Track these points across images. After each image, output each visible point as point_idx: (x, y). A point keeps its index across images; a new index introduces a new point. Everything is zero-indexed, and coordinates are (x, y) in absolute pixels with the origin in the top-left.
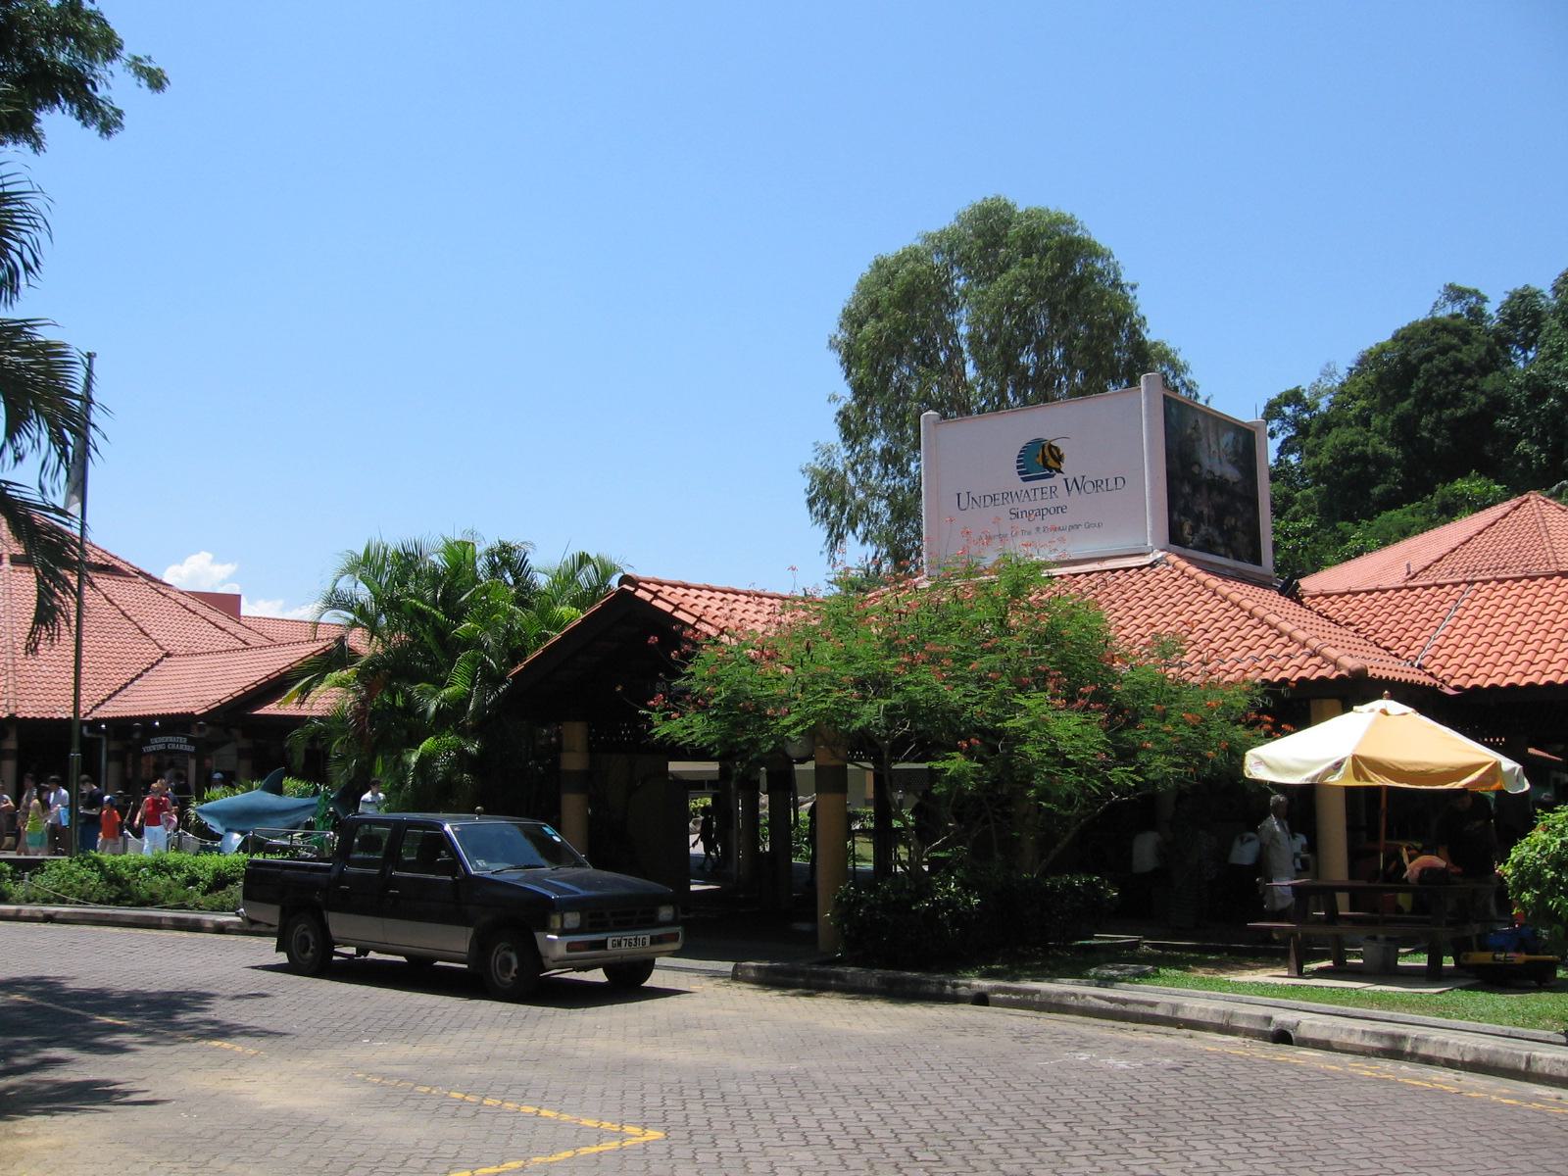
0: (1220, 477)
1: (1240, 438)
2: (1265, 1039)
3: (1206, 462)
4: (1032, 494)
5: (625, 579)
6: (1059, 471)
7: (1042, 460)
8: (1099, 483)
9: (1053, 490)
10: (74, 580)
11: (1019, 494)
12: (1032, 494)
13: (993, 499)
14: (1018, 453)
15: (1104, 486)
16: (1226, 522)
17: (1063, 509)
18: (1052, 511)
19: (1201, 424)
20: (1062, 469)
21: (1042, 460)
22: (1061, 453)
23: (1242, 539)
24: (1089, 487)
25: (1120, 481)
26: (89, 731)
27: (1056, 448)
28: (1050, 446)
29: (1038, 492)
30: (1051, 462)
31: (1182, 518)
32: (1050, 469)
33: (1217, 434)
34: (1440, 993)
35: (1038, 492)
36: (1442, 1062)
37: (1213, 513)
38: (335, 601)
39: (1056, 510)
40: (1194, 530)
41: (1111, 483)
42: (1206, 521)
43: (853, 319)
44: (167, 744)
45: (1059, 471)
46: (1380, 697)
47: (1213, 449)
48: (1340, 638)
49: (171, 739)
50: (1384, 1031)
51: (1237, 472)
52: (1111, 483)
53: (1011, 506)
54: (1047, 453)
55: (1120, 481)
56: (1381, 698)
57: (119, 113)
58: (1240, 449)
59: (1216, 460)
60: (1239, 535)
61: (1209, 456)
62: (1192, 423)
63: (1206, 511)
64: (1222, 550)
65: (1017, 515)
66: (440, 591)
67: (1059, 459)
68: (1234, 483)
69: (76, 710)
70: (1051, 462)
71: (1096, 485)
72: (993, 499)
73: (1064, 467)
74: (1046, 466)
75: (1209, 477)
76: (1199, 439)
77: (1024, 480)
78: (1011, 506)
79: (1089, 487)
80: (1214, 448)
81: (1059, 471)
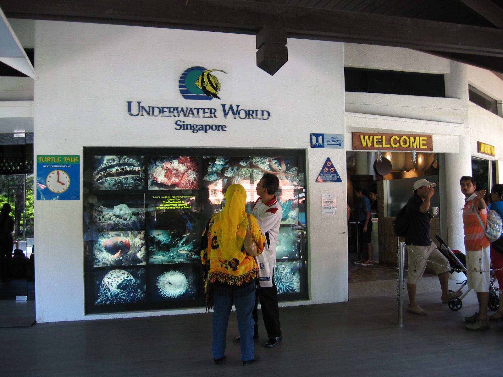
5: (153, 187)
10: (196, 250)
13: (161, 110)
15: (254, 115)
17: (222, 128)
20: (218, 95)
22: (434, 158)
24: (242, 114)
25: (266, 114)
27: (213, 77)
34: (276, 345)
36: (302, 176)
38: (32, 214)
41: (259, 114)
53: (177, 119)
54: (206, 79)
55: (266, 114)
66: (203, 207)
69: (502, 290)
71: (248, 113)
78: (177, 119)
79: (242, 114)
81: (216, 96)
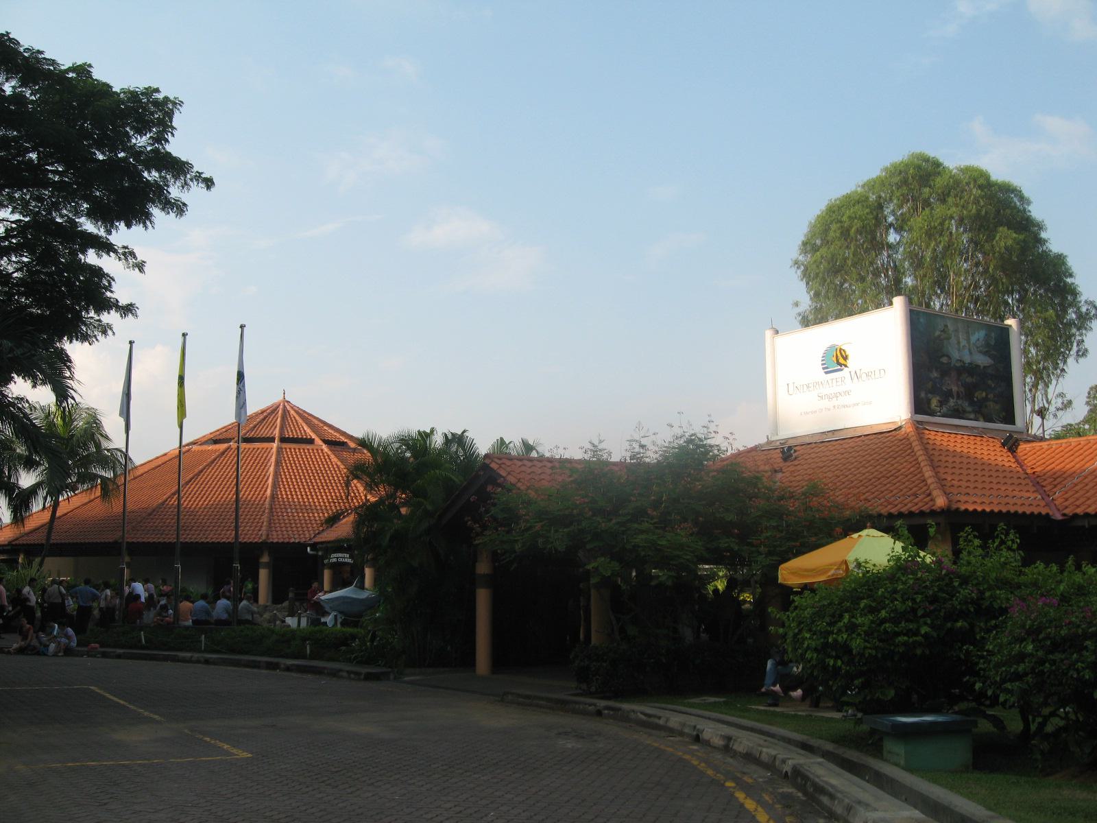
0: (970, 364)
1: (993, 335)
2: (797, 746)
3: (955, 355)
4: (830, 382)
6: (846, 366)
7: (837, 359)
8: (870, 374)
9: (843, 380)
11: (823, 382)
12: (830, 382)
14: (822, 355)
16: (976, 395)
17: (848, 393)
18: (842, 394)
19: (951, 327)
21: (837, 359)
23: (993, 407)
25: (882, 372)
26: (311, 550)
27: (844, 350)
28: (841, 349)
29: (834, 381)
30: (841, 361)
31: (929, 395)
32: (841, 365)
33: (968, 333)
35: (834, 381)
37: (962, 390)
39: (845, 392)
40: (941, 403)
41: (877, 373)
42: (955, 396)
43: (808, 246)
44: (337, 558)
45: (846, 366)
46: (865, 528)
47: (962, 345)
48: (973, 479)
49: (340, 555)
50: (733, 728)
51: (988, 358)
52: (877, 373)
55: (882, 372)
56: (866, 528)
57: (185, 205)
58: (992, 342)
59: (966, 351)
60: (991, 404)
61: (959, 350)
62: (941, 327)
63: (955, 389)
64: (972, 416)
65: (821, 397)
67: (845, 358)
68: (984, 367)
70: (841, 361)
72: (808, 387)
73: (849, 363)
74: (841, 365)
75: (958, 364)
76: (948, 338)
77: (826, 373)
80: (963, 343)
